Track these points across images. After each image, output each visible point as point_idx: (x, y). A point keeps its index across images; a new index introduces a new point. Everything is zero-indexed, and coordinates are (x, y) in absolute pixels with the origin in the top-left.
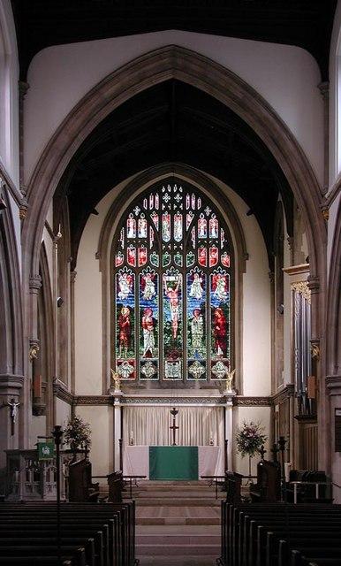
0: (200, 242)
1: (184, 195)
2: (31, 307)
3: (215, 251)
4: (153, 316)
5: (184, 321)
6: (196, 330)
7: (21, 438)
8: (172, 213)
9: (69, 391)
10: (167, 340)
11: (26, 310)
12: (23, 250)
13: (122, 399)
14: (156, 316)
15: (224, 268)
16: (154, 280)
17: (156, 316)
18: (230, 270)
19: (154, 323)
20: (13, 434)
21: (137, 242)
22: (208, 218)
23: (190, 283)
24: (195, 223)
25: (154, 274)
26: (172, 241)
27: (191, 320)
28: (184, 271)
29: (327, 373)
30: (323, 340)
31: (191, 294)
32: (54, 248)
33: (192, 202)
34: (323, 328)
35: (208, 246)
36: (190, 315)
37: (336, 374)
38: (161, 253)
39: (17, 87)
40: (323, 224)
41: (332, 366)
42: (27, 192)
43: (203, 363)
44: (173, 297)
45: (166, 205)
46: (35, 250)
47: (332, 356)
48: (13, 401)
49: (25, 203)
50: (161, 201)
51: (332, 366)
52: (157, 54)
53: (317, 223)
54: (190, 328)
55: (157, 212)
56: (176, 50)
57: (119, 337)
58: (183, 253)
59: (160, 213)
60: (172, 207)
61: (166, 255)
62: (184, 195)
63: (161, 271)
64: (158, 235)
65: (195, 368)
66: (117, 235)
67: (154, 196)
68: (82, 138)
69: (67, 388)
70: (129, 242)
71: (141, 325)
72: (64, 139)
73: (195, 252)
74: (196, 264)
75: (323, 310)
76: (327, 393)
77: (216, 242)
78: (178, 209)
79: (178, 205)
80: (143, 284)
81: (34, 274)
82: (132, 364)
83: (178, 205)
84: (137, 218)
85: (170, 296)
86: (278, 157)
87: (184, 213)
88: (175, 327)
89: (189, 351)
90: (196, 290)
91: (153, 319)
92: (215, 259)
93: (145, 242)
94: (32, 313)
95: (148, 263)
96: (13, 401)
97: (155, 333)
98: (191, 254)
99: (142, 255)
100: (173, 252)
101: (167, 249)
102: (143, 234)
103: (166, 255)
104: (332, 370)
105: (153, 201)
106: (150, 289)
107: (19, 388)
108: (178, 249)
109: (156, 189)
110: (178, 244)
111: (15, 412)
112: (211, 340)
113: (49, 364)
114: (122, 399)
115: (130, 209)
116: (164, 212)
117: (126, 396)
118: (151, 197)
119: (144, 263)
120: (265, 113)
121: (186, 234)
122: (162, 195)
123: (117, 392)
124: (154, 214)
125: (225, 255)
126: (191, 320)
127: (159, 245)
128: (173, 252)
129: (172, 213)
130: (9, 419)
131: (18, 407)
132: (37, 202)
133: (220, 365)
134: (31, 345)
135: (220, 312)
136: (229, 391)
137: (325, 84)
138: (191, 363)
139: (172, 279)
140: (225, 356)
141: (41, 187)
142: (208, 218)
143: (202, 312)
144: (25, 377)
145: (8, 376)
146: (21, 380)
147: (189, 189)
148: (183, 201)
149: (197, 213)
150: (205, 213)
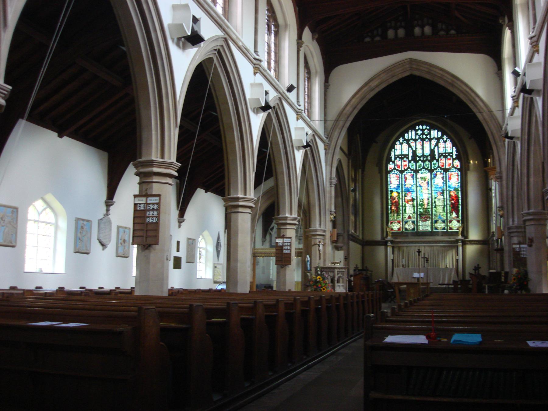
0: (440, 155)
1: (430, 130)
3: (450, 159)
5: (432, 201)
6: (439, 203)
8: (423, 140)
10: (420, 210)
11: (328, 195)
12: (326, 165)
13: (392, 242)
14: (414, 196)
16: (413, 177)
17: (414, 196)
19: (413, 200)
20: (320, 259)
23: (435, 177)
24: (437, 145)
25: (412, 173)
26: (423, 155)
27: (436, 198)
28: (431, 171)
30: (505, 206)
31: (435, 184)
33: (435, 133)
34: (505, 201)
35: (445, 157)
37: (513, 224)
38: (416, 162)
39: (323, 86)
41: (511, 220)
43: (444, 222)
44: (424, 184)
45: (419, 136)
47: (510, 215)
48: (320, 242)
49: (327, 141)
50: (416, 134)
51: (511, 220)
53: (499, 144)
54: (435, 202)
55: (414, 140)
56: (412, 61)
58: (430, 161)
59: (415, 140)
61: (420, 163)
62: (430, 130)
63: (416, 171)
64: (414, 152)
65: (438, 224)
69: (359, 236)
71: (405, 202)
72: (349, 108)
74: (439, 167)
75: (505, 190)
78: (426, 138)
79: (426, 135)
80: (406, 179)
82: (399, 223)
83: (426, 135)
85: (422, 185)
86: (475, 110)
87: (430, 140)
88: (426, 202)
89: (435, 215)
92: (450, 164)
93: (407, 156)
95: (409, 168)
96: (320, 242)
97: (413, 206)
99: (405, 163)
100: (423, 161)
102: (405, 152)
103: (420, 163)
104: (511, 223)
105: (411, 134)
106: (410, 182)
107: (323, 235)
108: (427, 160)
110: (427, 157)
111: (321, 248)
114: (392, 242)
115: (397, 139)
116: (417, 140)
118: (410, 133)
119: (406, 168)
120: (465, 88)
121: (432, 151)
122: (416, 131)
123: (389, 238)
124: (412, 141)
125: (456, 161)
126: (436, 198)
127: (415, 158)
128: (423, 161)
129: (423, 140)
130: (318, 252)
131: (323, 245)
132: (334, 141)
133: (455, 222)
134: (330, 213)
135: (454, 193)
136: (460, 237)
138: (436, 222)
139: (423, 176)
140: (458, 217)
141: (336, 134)
142: (445, 142)
146: (325, 231)
148: (430, 134)
149: (438, 139)
150: (443, 139)
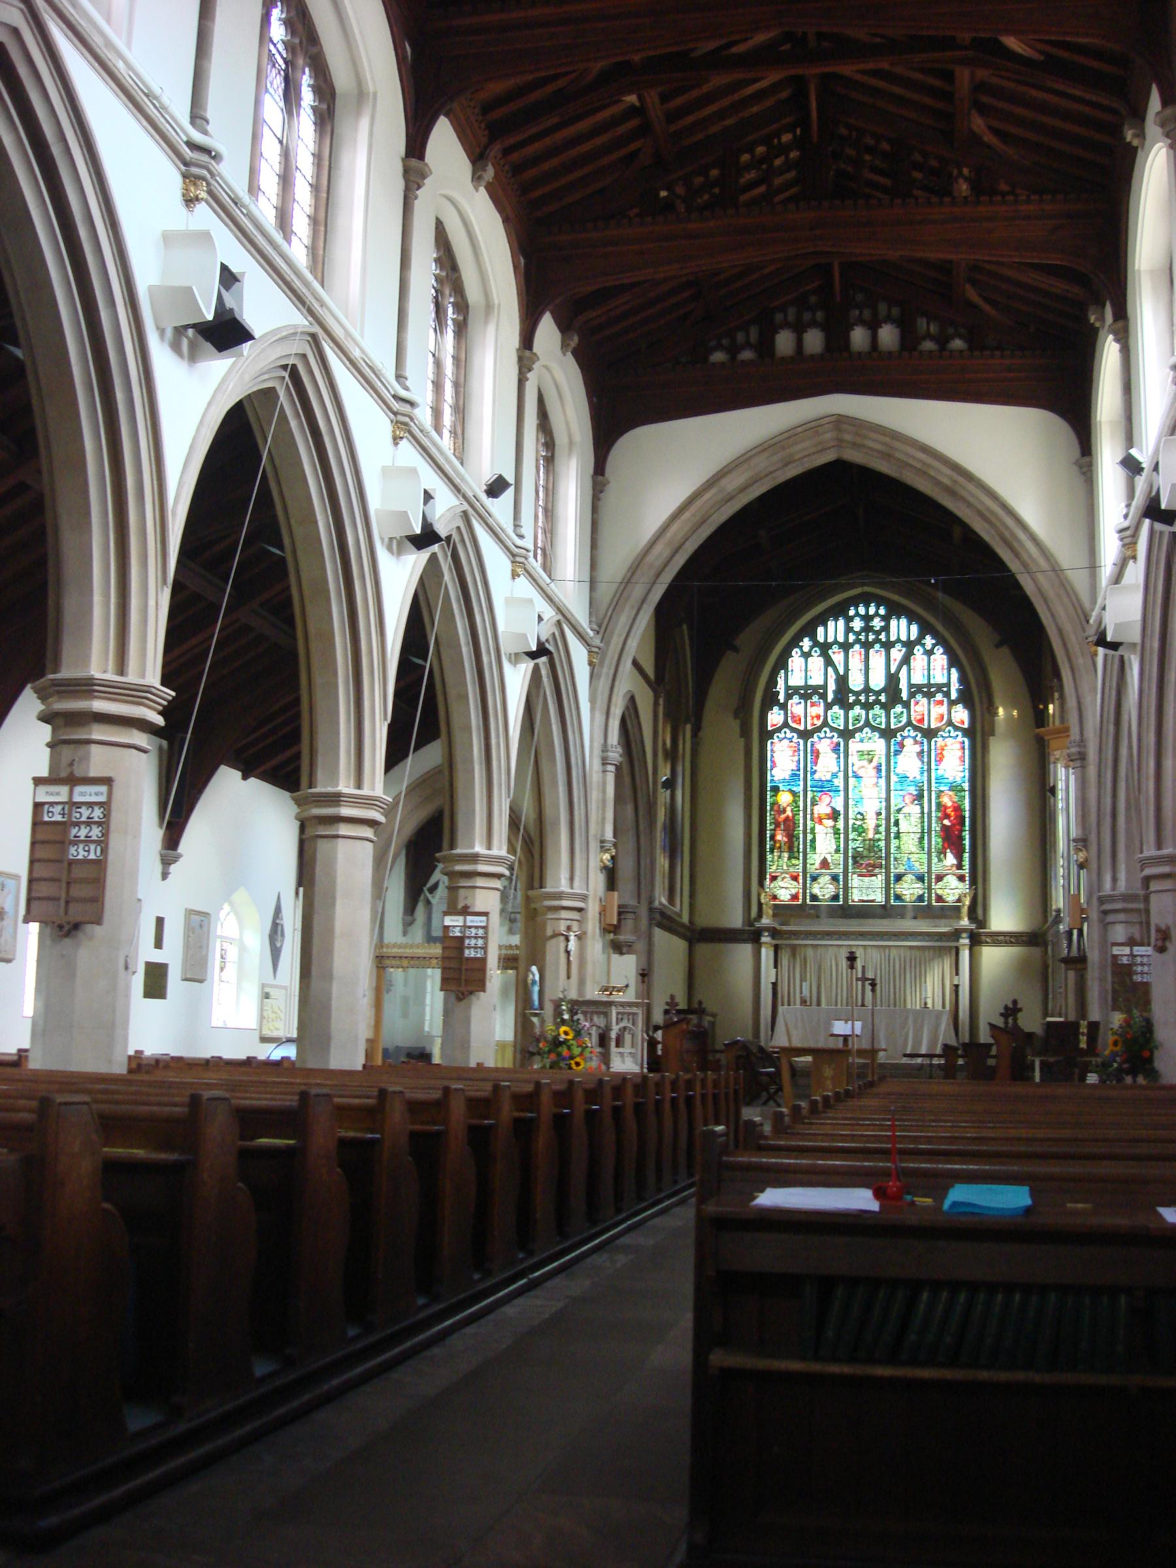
0: (916, 690)
2: (604, 792)
3: (941, 703)
4: (833, 804)
7: (582, 982)
8: (867, 646)
9: (685, 919)
11: (594, 795)
13: (774, 933)
14: (839, 804)
15: (956, 728)
16: (836, 749)
17: (839, 804)
18: (969, 733)
19: (834, 815)
20: (569, 977)
21: (806, 691)
22: (929, 653)
25: (835, 740)
26: (867, 690)
27: (899, 811)
28: (888, 734)
29: (1100, 889)
30: (1093, 838)
32: (656, 704)
33: (901, 628)
36: (895, 802)
37: (1114, 889)
38: (847, 707)
40: (1090, 661)
42: (600, 626)
44: (868, 772)
46: (612, 709)
50: (849, 629)
52: (812, 427)
54: (897, 823)
56: (840, 422)
57: (773, 837)
58: (887, 707)
59: (846, 647)
60: (867, 636)
61: (857, 710)
63: (847, 734)
64: (842, 681)
65: (905, 885)
66: (772, 682)
67: (836, 620)
68: (690, 548)
70: (791, 692)
71: (812, 819)
73: (907, 705)
74: (909, 723)
76: (1101, 921)
77: (944, 688)
78: (877, 640)
80: (816, 754)
81: (609, 742)
82: (795, 878)
83: (878, 633)
84: (806, 655)
89: (896, 859)
90: (908, 763)
91: (834, 809)
94: (604, 801)
96: (569, 928)
97: (836, 832)
98: (899, 708)
99: (813, 711)
100: (867, 706)
101: (857, 702)
103: (857, 710)
106: (828, 764)
107: (580, 910)
108: (877, 702)
109: (839, 611)
111: (573, 945)
112: (937, 841)
113: (642, 877)
114: (774, 933)
115: (795, 642)
116: (851, 645)
117: (785, 928)
118: (831, 624)
122: (849, 620)
123: (766, 921)
124: (835, 648)
126: (899, 811)
128: (867, 706)
129: (867, 646)
130: (563, 956)
134: (602, 847)
136: (965, 922)
137: (1086, 459)
139: (866, 747)
141: (623, 620)
142: (929, 653)
143: (919, 797)
144: (591, 893)
145: (562, 893)
146: (584, 898)
147: (895, 611)
148: (886, 629)
149: (910, 645)
